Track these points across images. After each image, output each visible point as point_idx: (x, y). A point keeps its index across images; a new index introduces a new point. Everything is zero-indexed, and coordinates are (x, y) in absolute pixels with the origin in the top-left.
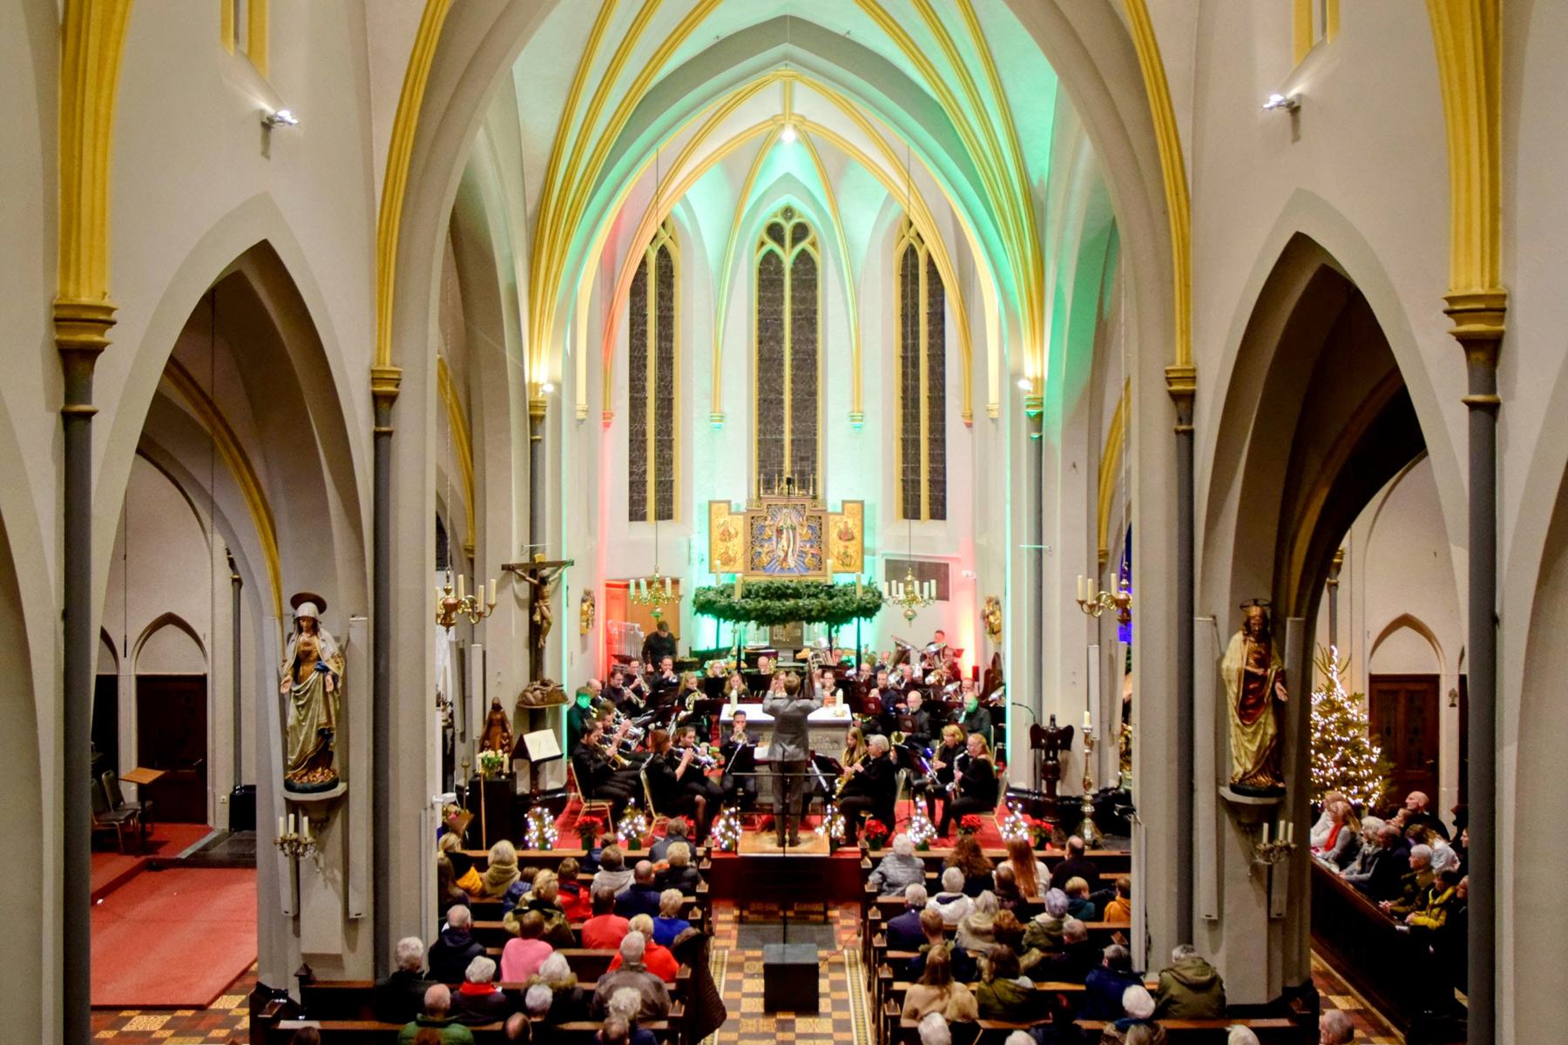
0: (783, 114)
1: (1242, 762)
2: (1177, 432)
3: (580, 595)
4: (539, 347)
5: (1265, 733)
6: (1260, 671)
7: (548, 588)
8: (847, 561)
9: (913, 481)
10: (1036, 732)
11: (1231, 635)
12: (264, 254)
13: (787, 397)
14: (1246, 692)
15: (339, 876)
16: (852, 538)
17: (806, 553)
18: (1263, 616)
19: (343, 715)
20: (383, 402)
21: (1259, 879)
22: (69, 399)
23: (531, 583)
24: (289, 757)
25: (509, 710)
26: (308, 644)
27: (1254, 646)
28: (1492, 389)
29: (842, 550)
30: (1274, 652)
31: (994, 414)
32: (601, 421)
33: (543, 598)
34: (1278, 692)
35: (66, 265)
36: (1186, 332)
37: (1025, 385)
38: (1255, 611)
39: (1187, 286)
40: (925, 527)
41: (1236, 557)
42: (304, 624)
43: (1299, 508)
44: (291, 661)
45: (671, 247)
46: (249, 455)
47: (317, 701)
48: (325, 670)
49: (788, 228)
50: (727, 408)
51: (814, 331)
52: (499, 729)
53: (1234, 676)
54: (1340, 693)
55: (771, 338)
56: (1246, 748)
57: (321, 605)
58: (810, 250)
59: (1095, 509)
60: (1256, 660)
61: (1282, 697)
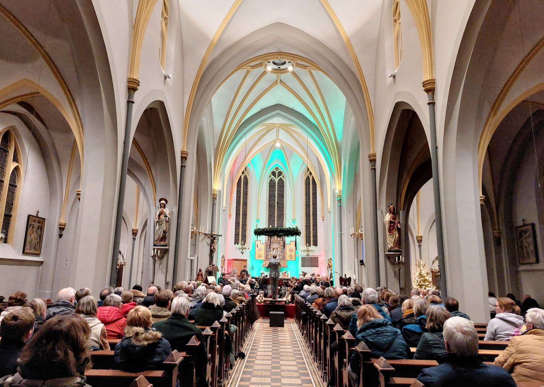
0: (277, 139)
1: (390, 245)
2: (372, 169)
3: (222, 256)
4: (216, 180)
5: (395, 237)
6: (394, 221)
7: (215, 241)
8: (291, 257)
9: (308, 225)
10: (341, 279)
11: (386, 213)
12: (162, 104)
13: (276, 215)
14: (390, 226)
15: (165, 271)
16: (293, 251)
17: (280, 255)
18: (394, 208)
19: (169, 229)
20: (184, 158)
21: (397, 277)
22: (129, 98)
23: (211, 239)
24: (155, 238)
25: (203, 272)
26: (162, 210)
27: (392, 215)
28: (433, 100)
29: (290, 254)
30: (397, 217)
31: (329, 210)
32: (228, 217)
33: (214, 243)
34: (398, 226)
35: (131, 70)
36: (373, 146)
37: (337, 192)
38: (392, 207)
39: (373, 136)
40: (312, 247)
41: (386, 199)
42: (162, 205)
43: (402, 185)
44: (158, 214)
45: (248, 176)
46: (151, 169)
47: (164, 224)
48: (166, 216)
49: (277, 172)
50: (260, 217)
51: (283, 198)
52: (201, 277)
53: (387, 222)
54: (423, 272)
55: (272, 200)
56: (391, 240)
57: (166, 202)
58: (282, 178)
59: (355, 224)
60: (392, 218)
61: (399, 227)
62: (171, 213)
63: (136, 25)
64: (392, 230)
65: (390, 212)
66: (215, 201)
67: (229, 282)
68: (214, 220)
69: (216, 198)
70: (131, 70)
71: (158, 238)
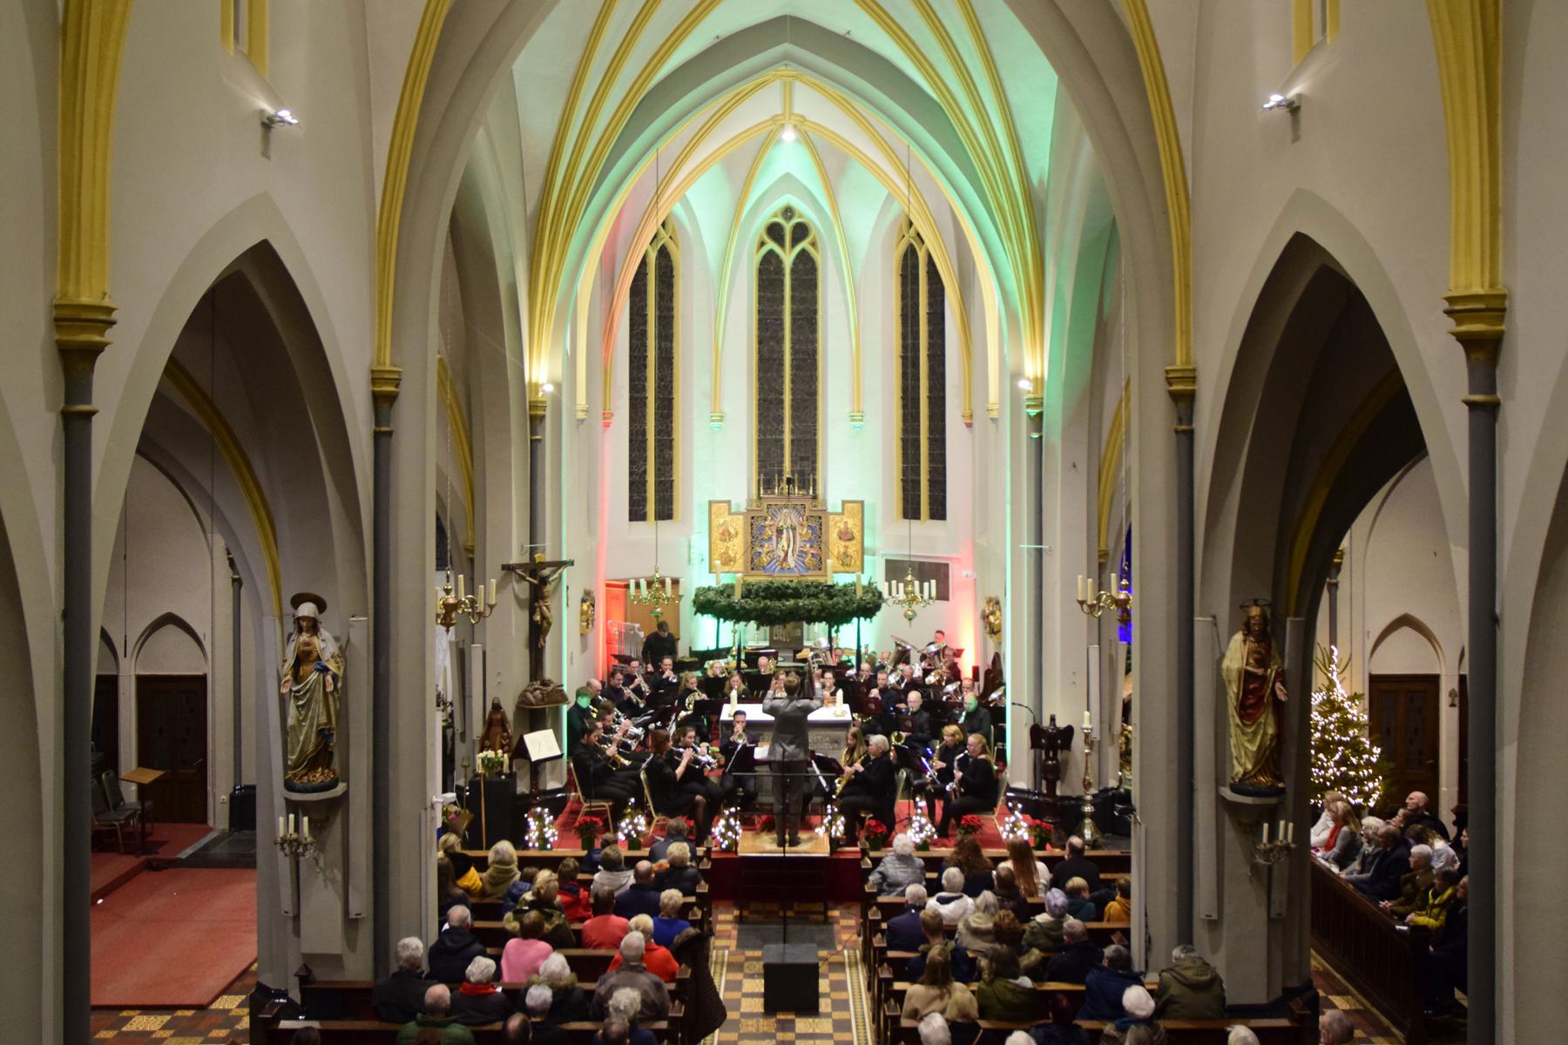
1: (1241, 766)
2: (1177, 432)
3: (580, 595)
5: (1265, 733)
6: (1260, 671)
7: (549, 588)
9: (913, 481)
11: (1231, 634)
13: (787, 397)
14: (1246, 692)
15: (339, 877)
17: (806, 553)
20: (383, 402)
23: (531, 583)
25: (509, 710)
28: (1492, 389)
29: (842, 550)
30: (1274, 652)
31: (994, 414)
32: (601, 421)
34: (1278, 692)
35: (66, 265)
36: (1186, 332)
37: (1025, 385)
38: (1255, 611)
40: (925, 527)
42: (304, 624)
44: (291, 661)
45: (671, 247)
47: (317, 702)
49: (788, 227)
51: (814, 330)
53: (1234, 676)
55: (771, 338)
56: (1246, 748)
57: (321, 605)
62: (343, 653)
63: (72, 17)
64: (1250, 706)
65: (1248, 631)
66: (539, 429)
67: (609, 758)
68: (539, 493)
69: (543, 417)
70: (66, 265)
71: (298, 758)
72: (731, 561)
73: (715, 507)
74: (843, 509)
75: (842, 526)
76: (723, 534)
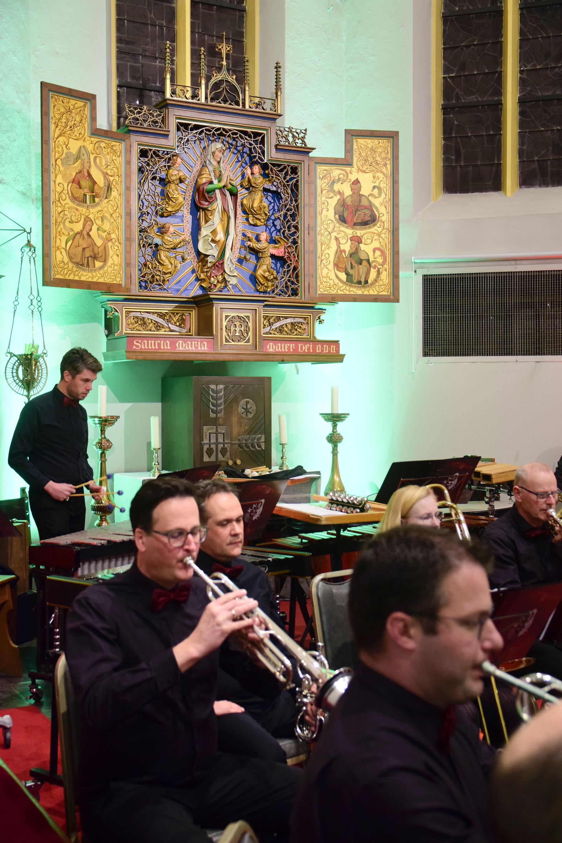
29: (347, 247)
72: (95, 257)
73: (384, 144)
74: (349, 150)
75: (348, 192)
76: (76, 182)
